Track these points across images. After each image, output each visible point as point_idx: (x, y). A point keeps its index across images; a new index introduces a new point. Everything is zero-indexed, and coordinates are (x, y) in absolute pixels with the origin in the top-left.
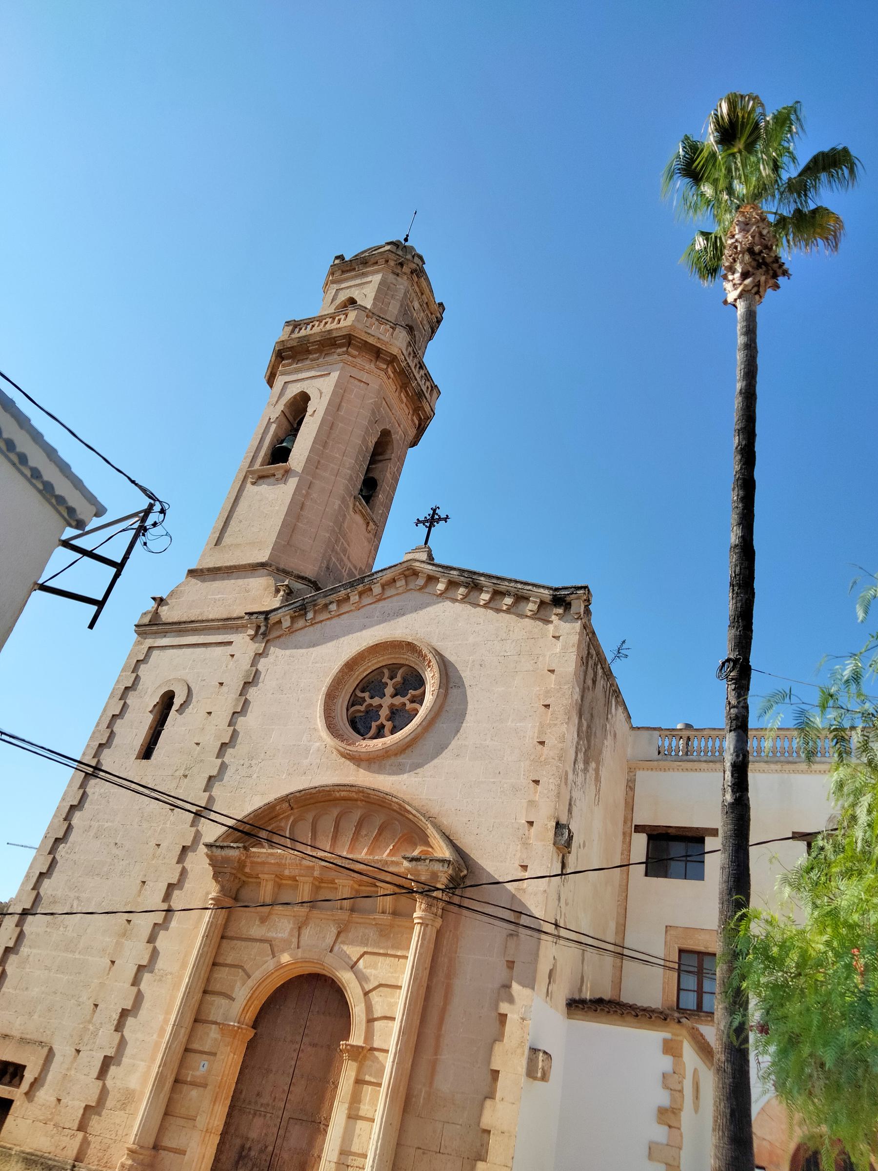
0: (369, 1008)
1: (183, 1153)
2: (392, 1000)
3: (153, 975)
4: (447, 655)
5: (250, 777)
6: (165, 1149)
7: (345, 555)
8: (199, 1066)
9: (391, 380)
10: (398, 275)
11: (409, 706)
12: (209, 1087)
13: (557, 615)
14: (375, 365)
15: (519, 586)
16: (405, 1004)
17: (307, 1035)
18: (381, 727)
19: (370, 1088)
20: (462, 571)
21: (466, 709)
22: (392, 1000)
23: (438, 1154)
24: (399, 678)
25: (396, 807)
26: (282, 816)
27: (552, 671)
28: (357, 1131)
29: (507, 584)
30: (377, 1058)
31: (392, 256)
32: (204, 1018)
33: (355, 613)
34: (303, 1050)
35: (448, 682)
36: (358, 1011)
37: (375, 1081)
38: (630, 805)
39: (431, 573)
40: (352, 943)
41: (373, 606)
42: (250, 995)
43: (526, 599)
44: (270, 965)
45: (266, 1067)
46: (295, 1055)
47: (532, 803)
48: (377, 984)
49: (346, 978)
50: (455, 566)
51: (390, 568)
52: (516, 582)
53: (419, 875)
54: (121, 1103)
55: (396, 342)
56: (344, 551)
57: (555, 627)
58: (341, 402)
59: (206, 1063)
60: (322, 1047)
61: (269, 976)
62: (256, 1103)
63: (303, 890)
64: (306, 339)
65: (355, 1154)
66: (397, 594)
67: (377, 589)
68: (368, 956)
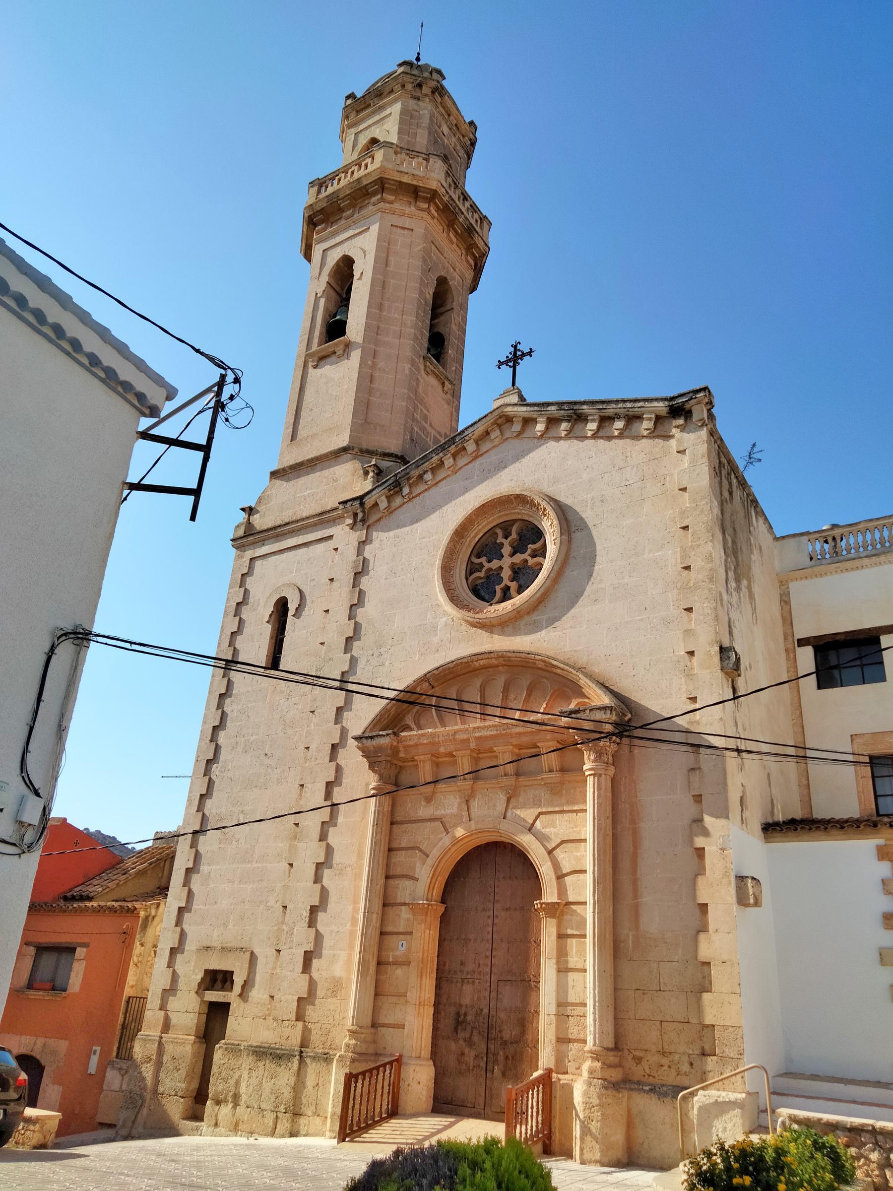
0: (556, 865)
2: (579, 854)
3: (333, 870)
4: (562, 498)
6: (384, 1025)
7: (426, 422)
9: (435, 220)
10: (418, 99)
11: (531, 562)
12: (413, 964)
13: (677, 427)
14: (415, 206)
15: (629, 405)
16: (594, 855)
17: (498, 901)
18: (507, 589)
19: (574, 940)
20: (560, 404)
21: (595, 551)
22: (579, 854)
24: (514, 535)
27: (684, 489)
28: (570, 983)
29: (614, 406)
30: (575, 911)
31: (408, 78)
33: (453, 478)
35: (569, 527)
36: (545, 870)
37: (578, 933)
38: (788, 620)
39: (526, 415)
40: (524, 806)
41: (470, 465)
42: (432, 872)
43: (639, 418)
44: (446, 841)
46: (490, 922)
47: (688, 633)
48: (559, 841)
49: (526, 841)
50: (551, 400)
51: (480, 420)
52: (624, 401)
55: (432, 174)
56: (425, 418)
57: (678, 440)
58: (388, 256)
59: (405, 943)
62: (461, 971)
63: (462, 763)
64: (335, 196)
65: (573, 1004)
66: (494, 447)
67: (471, 447)
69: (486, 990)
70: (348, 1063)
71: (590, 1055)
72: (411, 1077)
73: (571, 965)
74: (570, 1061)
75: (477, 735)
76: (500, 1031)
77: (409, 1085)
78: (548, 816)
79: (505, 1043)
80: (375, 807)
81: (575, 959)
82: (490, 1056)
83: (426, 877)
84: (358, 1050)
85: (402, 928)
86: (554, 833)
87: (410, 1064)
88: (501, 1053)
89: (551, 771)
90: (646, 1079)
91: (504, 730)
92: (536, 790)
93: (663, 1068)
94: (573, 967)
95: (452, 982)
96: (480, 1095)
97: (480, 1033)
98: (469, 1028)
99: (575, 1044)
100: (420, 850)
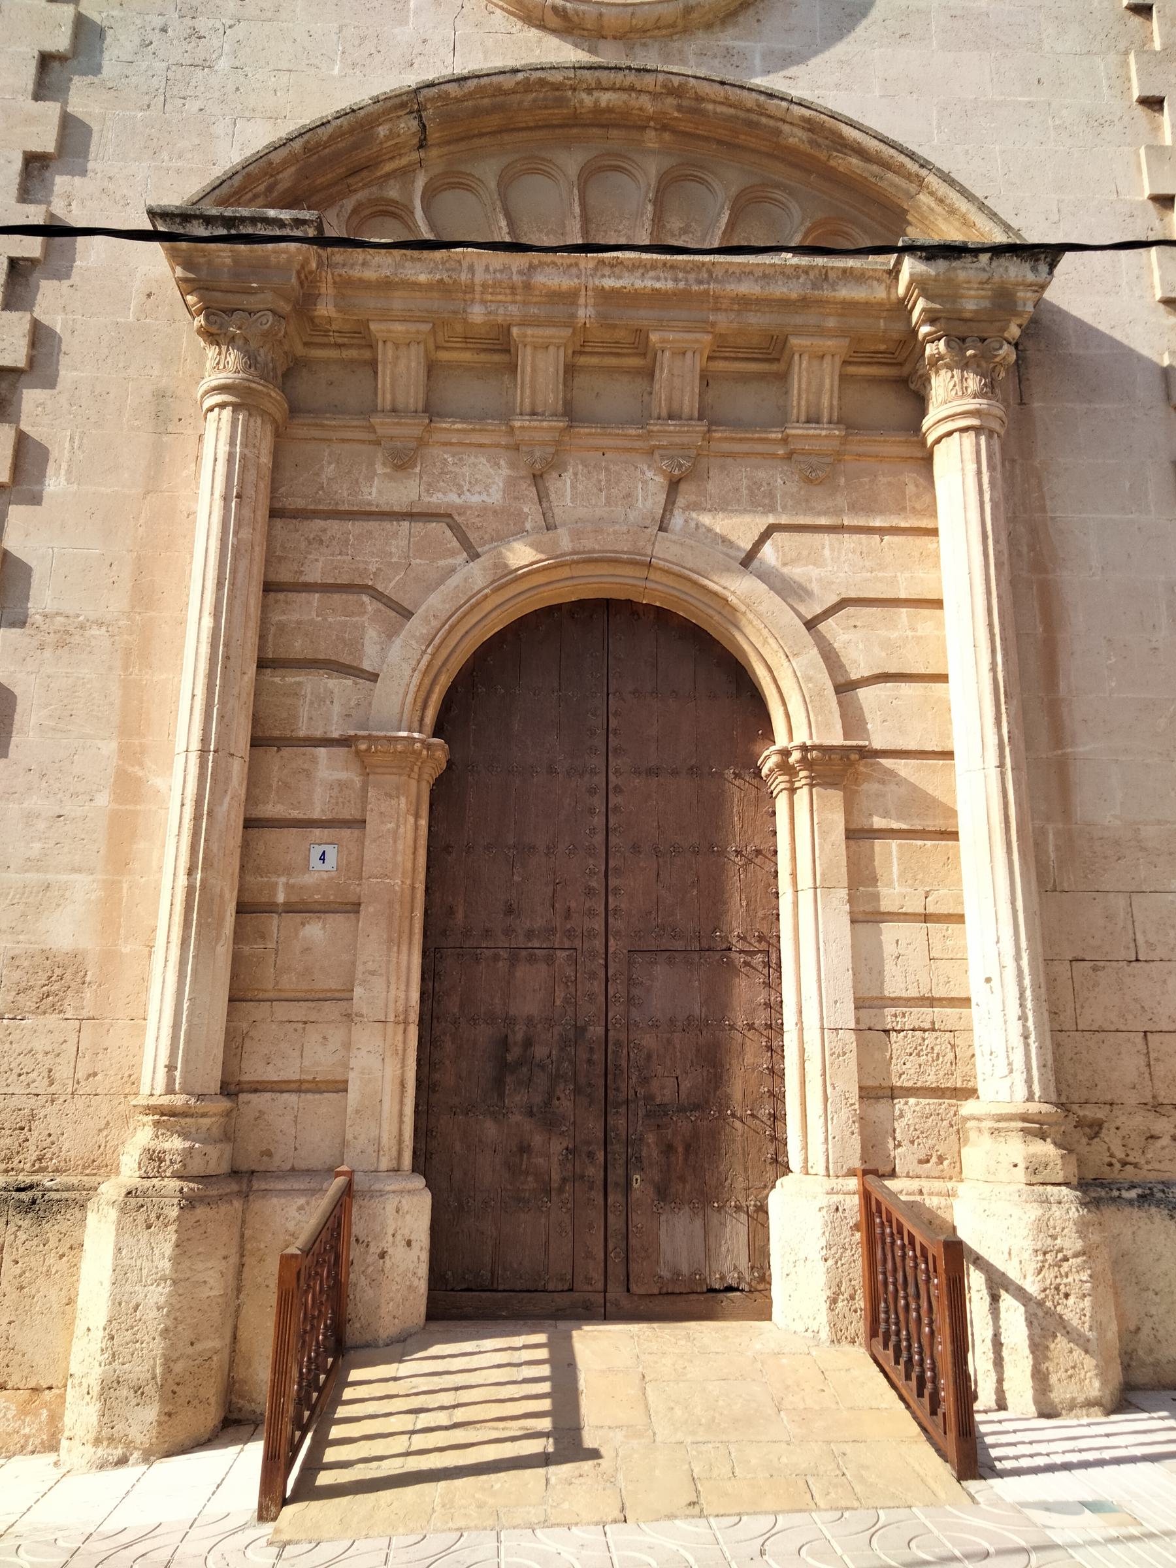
1: (341, 1087)
2: (894, 635)
3: (28, 630)
5: (206, 65)
6: (257, 1088)
8: (307, 859)
12: (367, 910)
16: (990, 625)
17: (618, 751)
19: (894, 844)
22: (894, 635)
23: (1134, 964)
25: (796, 137)
26: (388, 167)
28: (889, 949)
30: (891, 773)
32: (277, 733)
34: (616, 787)
37: (904, 826)
40: (723, 506)
42: (427, 658)
44: (476, 575)
45: (511, 840)
46: (598, 802)
48: (833, 599)
53: (955, 298)
54: (35, 994)
59: (332, 852)
60: (675, 773)
61: (478, 603)
62: (508, 931)
63: (534, 370)
65: (895, 1002)
68: (785, 535)
69: (593, 976)
70: (174, 1212)
71: (1021, 1125)
72: (390, 1231)
73: (886, 906)
74: (900, 1145)
75: (609, 283)
76: (645, 1081)
77: (382, 1255)
78: (798, 537)
79: (658, 1114)
80: (232, 443)
81: (898, 889)
82: (617, 1147)
83: (408, 672)
84: (196, 1167)
85: (318, 810)
86: (820, 580)
87: (382, 1193)
88: (651, 1138)
89: (813, 419)
90: (1115, 1174)
91: (700, 282)
92: (757, 467)
93: (1160, 1143)
94: (894, 909)
95: (477, 960)
96: (589, 1255)
97: (578, 1091)
98: (541, 1080)
99: (912, 1101)
100: (377, 595)
